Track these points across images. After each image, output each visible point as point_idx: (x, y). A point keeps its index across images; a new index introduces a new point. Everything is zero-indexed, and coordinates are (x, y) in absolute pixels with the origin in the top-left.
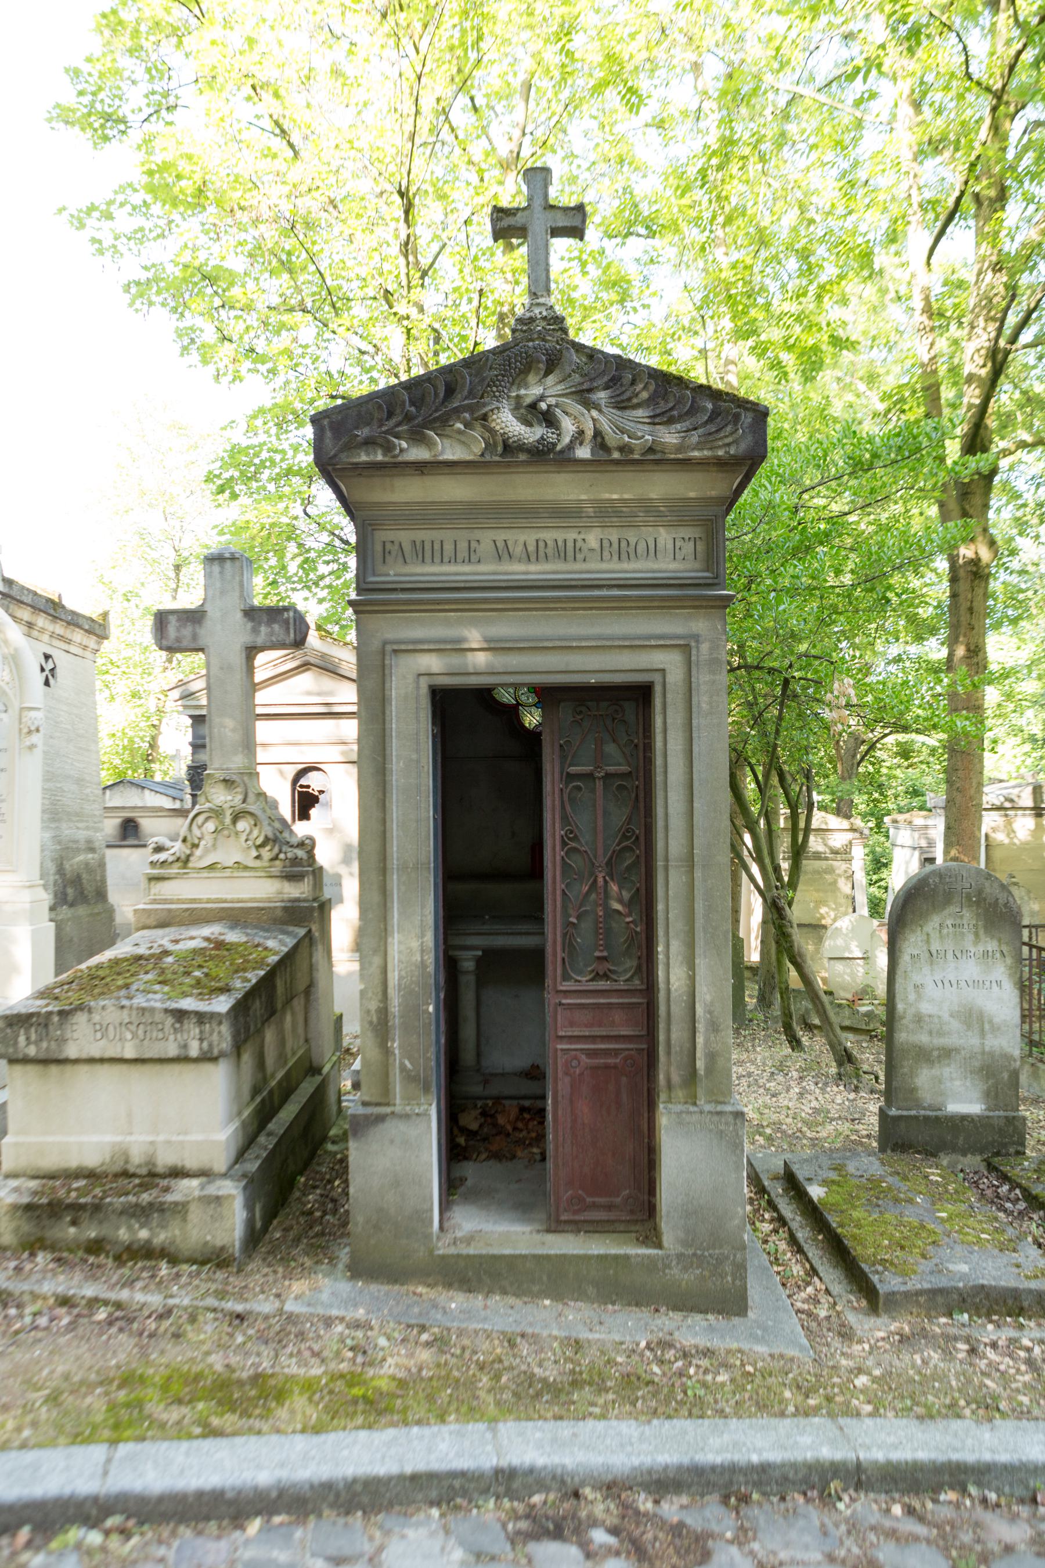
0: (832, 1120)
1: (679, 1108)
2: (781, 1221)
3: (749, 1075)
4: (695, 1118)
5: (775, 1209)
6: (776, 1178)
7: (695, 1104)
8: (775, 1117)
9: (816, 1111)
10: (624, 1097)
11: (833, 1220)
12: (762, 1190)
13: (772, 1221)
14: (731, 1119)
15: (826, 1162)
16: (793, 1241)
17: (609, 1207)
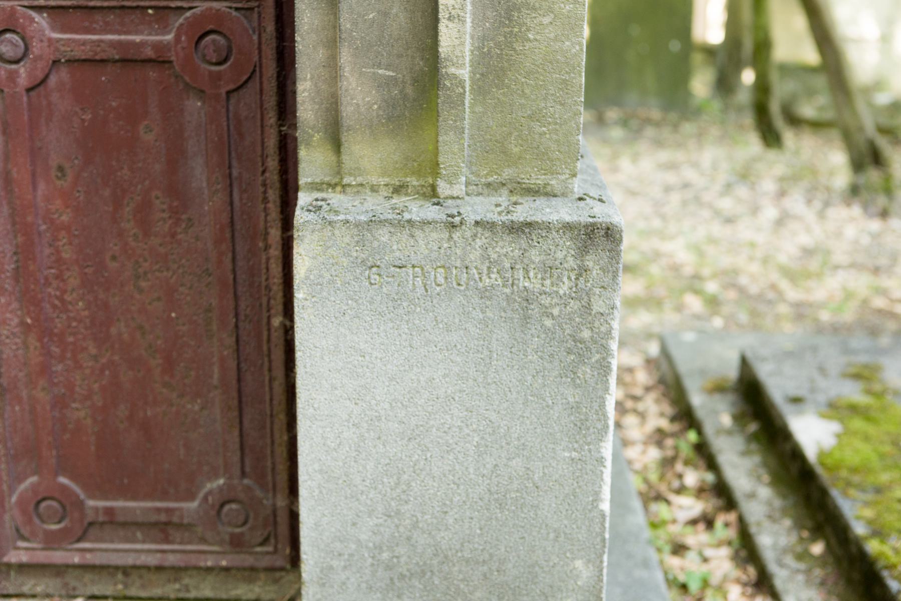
0: (837, 267)
1: (375, 204)
2: (722, 493)
3: (686, 186)
4: (427, 244)
5: (712, 464)
6: (719, 389)
7: (432, 194)
8: (727, 262)
9: (808, 252)
10: (199, 173)
11: (857, 514)
12: (686, 417)
13: (700, 491)
14: (564, 251)
15: (836, 362)
16: (747, 550)
17: (163, 528)
